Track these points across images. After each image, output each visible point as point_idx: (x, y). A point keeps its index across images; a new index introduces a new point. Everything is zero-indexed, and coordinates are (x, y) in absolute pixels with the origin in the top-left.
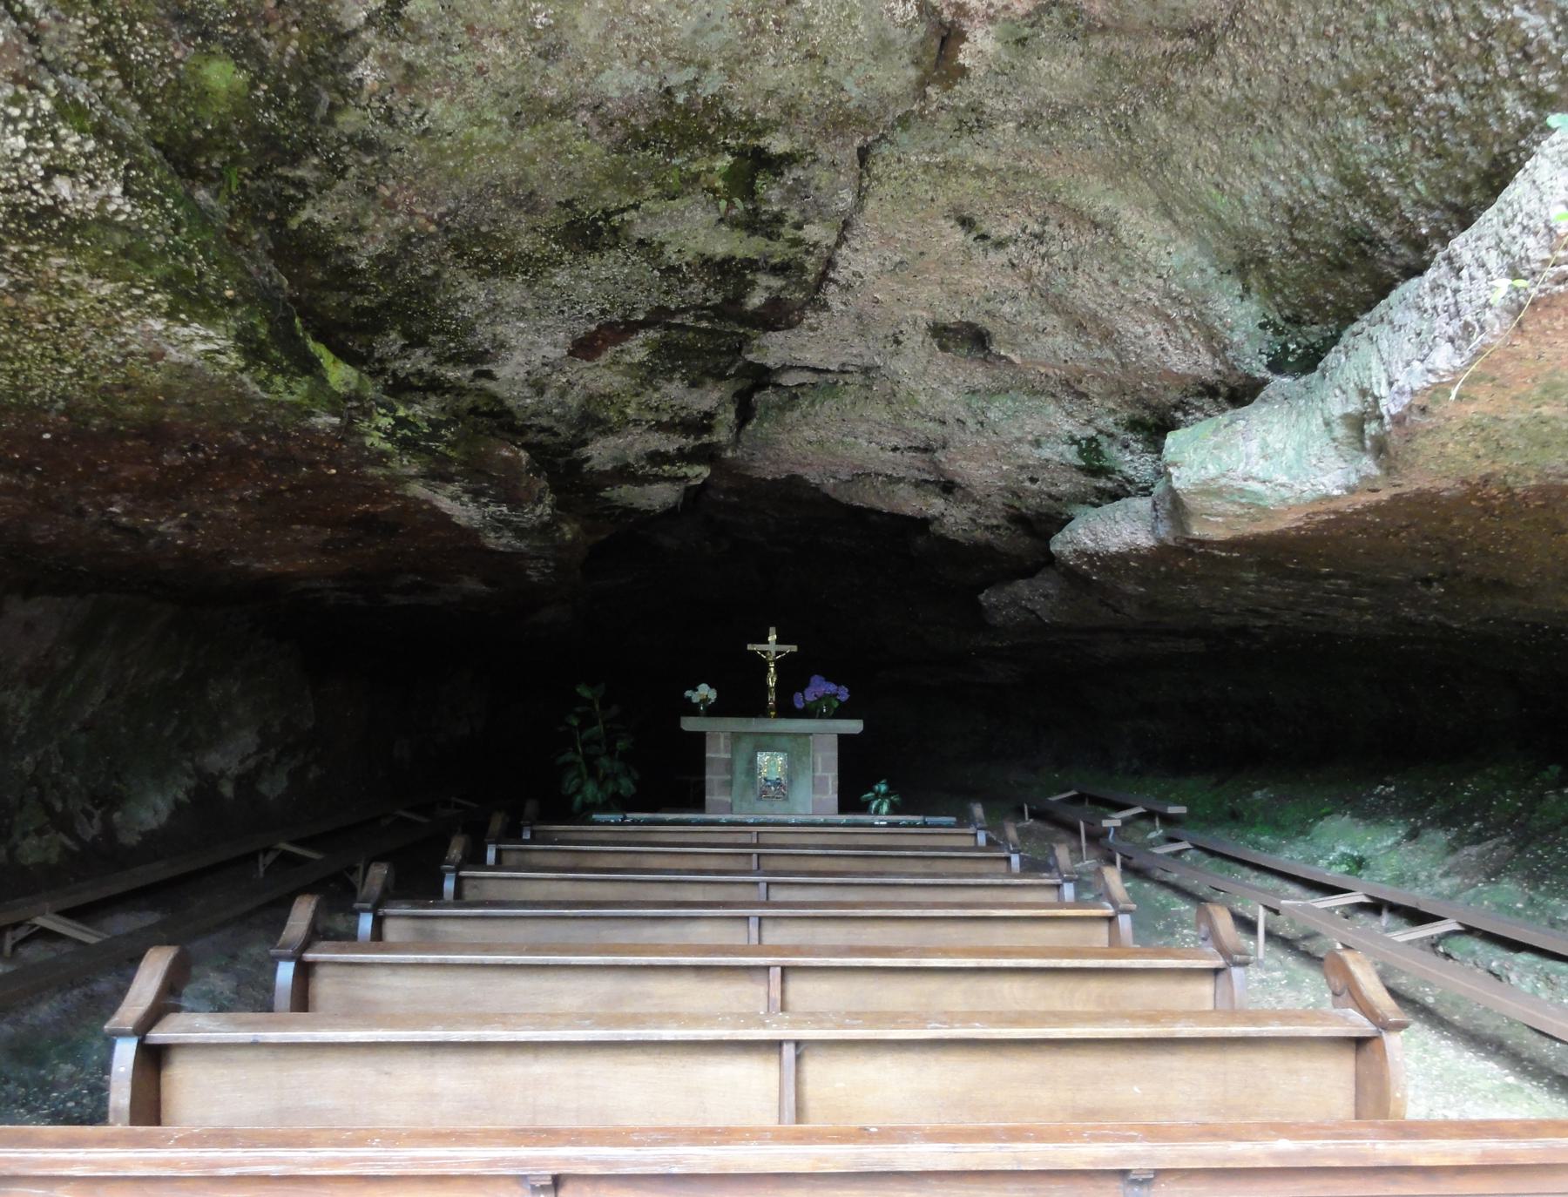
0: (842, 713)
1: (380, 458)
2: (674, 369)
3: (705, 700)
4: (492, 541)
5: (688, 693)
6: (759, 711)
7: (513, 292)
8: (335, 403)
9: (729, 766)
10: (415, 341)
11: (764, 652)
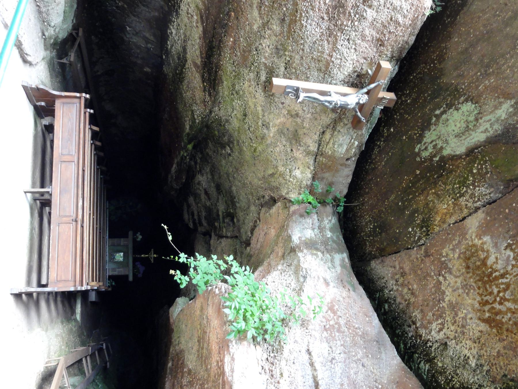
0: (134, 275)
1: (180, 153)
2: (207, 212)
3: (137, 238)
4: (170, 176)
5: (139, 233)
6: (134, 253)
7: (210, 176)
8: (185, 146)
9: (119, 245)
10: (201, 159)
11: (151, 253)
